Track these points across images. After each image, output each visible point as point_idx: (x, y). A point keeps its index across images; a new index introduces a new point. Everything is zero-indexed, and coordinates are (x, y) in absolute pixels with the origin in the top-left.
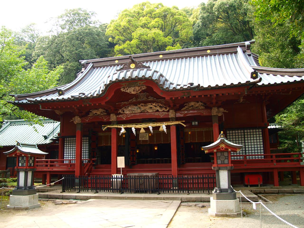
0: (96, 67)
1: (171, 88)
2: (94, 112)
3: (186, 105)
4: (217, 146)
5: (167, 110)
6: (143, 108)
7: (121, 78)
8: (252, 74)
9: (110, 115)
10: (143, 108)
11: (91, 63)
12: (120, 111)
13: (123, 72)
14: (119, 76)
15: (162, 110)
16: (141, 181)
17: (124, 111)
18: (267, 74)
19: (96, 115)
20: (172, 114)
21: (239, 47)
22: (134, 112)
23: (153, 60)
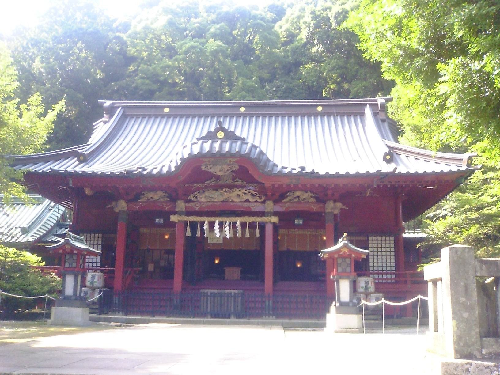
0: (129, 115)
2: (150, 195)
3: (289, 196)
4: (339, 251)
5: (262, 200)
6: (226, 195)
8: (386, 155)
9: (176, 203)
10: (226, 195)
11: (120, 108)
12: (191, 197)
13: (207, 142)
15: (254, 200)
16: (216, 300)
17: (196, 197)
18: (407, 157)
19: (151, 200)
20: (270, 206)
21: (368, 105)
22: (213, 200)
23: (229, 114)
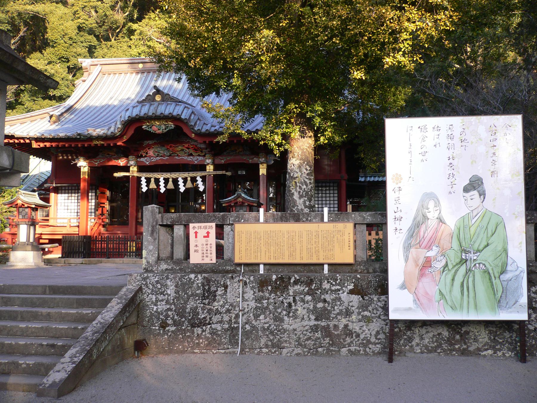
1: (203, 130)
7: (142, 114)
14: (140, 112)
